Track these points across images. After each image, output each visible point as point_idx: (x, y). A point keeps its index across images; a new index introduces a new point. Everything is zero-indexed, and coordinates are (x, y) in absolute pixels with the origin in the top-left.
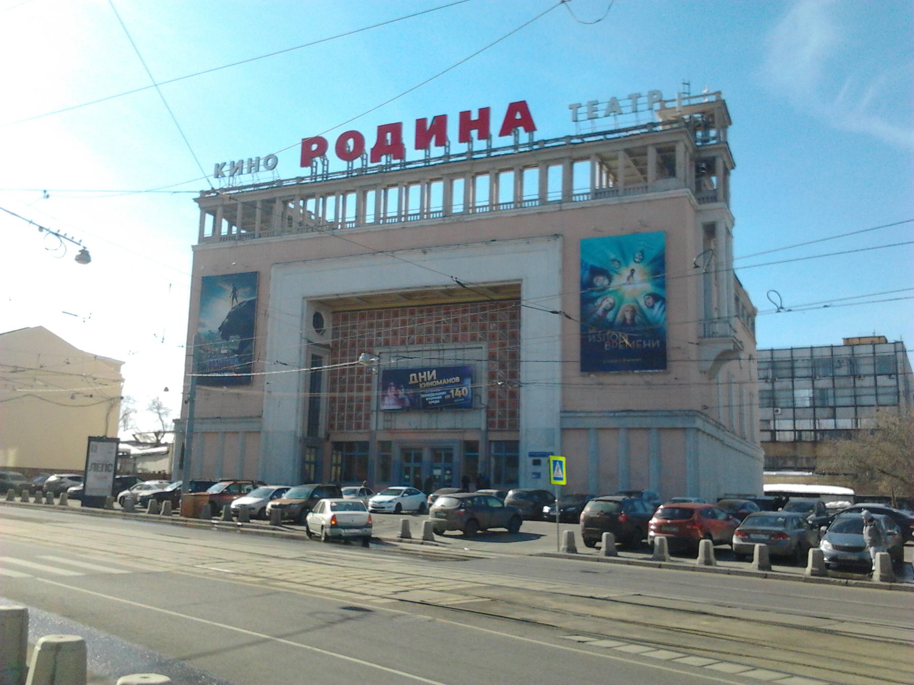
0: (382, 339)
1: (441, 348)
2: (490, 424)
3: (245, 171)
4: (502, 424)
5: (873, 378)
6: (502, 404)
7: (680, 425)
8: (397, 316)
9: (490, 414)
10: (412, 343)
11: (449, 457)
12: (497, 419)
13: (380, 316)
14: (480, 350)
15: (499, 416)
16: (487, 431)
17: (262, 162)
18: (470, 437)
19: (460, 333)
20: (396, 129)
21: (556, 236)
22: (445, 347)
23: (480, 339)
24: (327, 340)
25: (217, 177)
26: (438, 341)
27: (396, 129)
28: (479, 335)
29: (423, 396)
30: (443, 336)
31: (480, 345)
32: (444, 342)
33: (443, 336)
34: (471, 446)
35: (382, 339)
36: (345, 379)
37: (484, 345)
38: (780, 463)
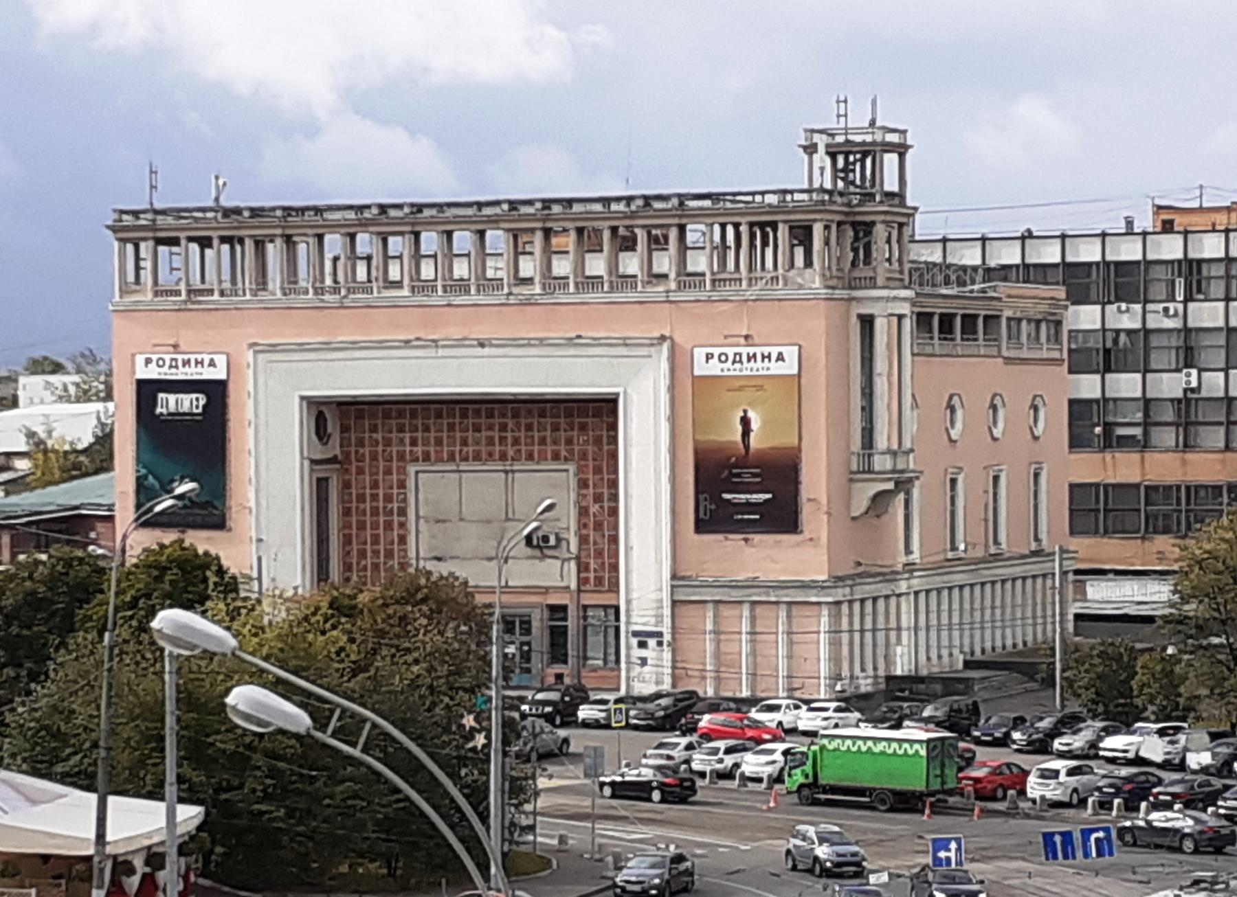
0: (419, 450)
1: (508, 468)
2: (582, 581)
4: (599, 581)
5: (455, 260)
6: (599, 554)
7: (813, 599)
8: (492, 416)
9: (582, 567)
10: (466, 459)
11: (527, 628)
12: (592, 575)
13: (490, 415)
14: (564, 474)
15: (595, 571)
16: (579, 591)
18: (554, 600)
19: (536, 448)
21: (663, 338)
22: (515, 468)
23: (566, 459)
24: (335, 449)
26: (503, 457)
28: (563, 453)
30: (484, 450)
31: (565, 467)
32: (513, 459)
33: (484, 450)
34: (558, 611)
35: (419, 450)
36: (392, 509)
37: (572, 468)
38: (938, 688)
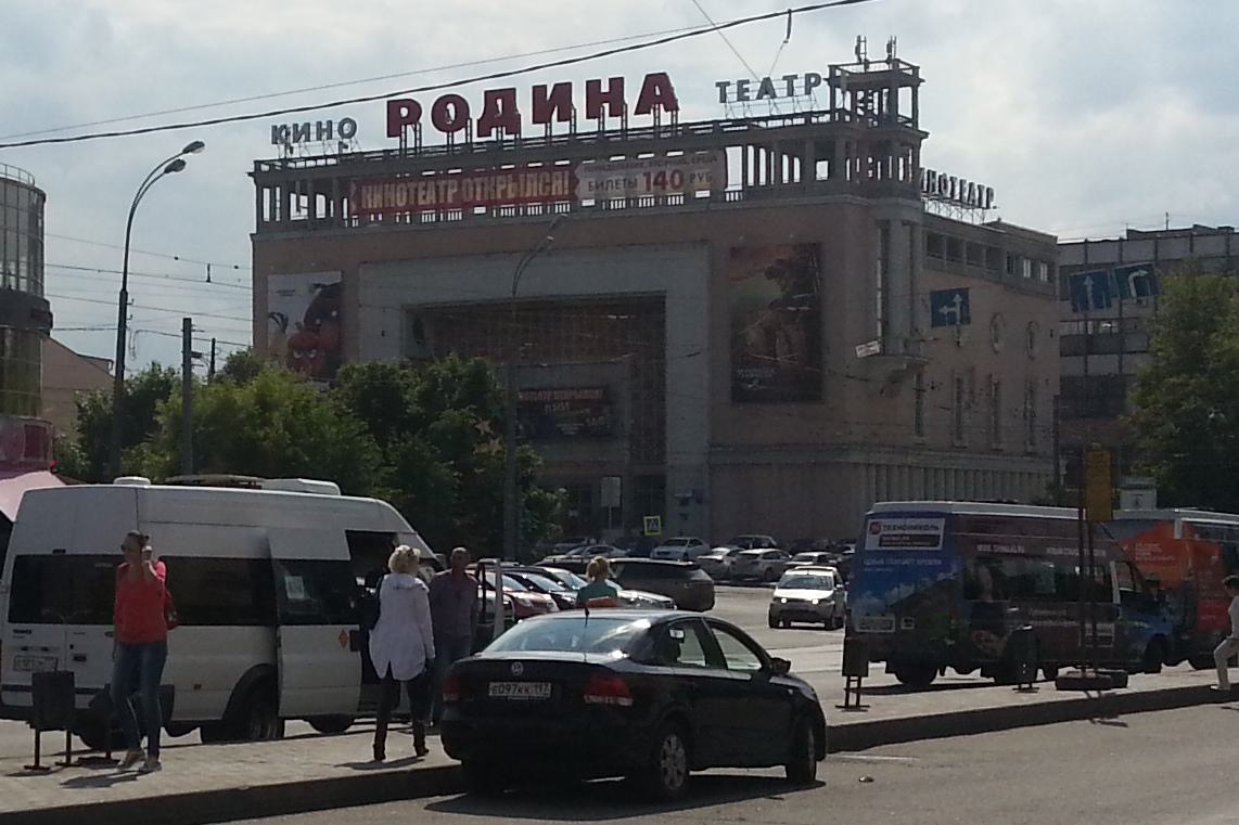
3: (313, 137)
17: (335, 127)
20: (509, 95)
25: (275, 142)
27: (509, 95)
29: (559, 425)
